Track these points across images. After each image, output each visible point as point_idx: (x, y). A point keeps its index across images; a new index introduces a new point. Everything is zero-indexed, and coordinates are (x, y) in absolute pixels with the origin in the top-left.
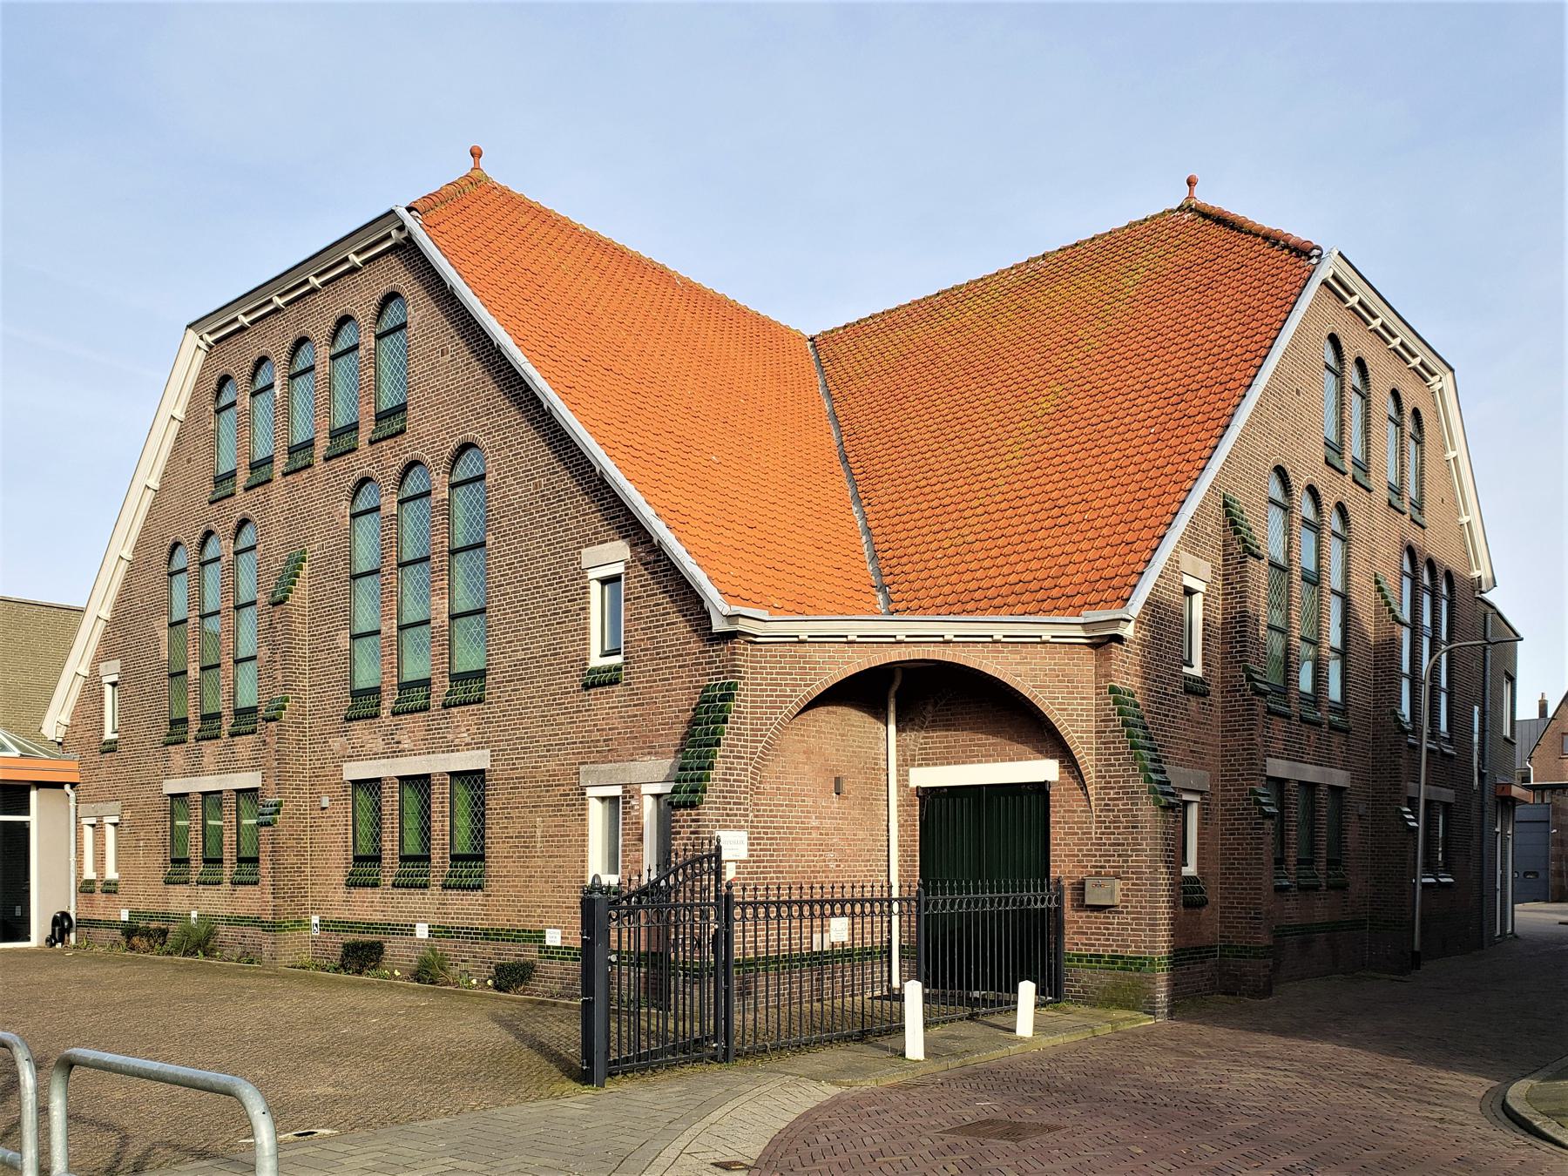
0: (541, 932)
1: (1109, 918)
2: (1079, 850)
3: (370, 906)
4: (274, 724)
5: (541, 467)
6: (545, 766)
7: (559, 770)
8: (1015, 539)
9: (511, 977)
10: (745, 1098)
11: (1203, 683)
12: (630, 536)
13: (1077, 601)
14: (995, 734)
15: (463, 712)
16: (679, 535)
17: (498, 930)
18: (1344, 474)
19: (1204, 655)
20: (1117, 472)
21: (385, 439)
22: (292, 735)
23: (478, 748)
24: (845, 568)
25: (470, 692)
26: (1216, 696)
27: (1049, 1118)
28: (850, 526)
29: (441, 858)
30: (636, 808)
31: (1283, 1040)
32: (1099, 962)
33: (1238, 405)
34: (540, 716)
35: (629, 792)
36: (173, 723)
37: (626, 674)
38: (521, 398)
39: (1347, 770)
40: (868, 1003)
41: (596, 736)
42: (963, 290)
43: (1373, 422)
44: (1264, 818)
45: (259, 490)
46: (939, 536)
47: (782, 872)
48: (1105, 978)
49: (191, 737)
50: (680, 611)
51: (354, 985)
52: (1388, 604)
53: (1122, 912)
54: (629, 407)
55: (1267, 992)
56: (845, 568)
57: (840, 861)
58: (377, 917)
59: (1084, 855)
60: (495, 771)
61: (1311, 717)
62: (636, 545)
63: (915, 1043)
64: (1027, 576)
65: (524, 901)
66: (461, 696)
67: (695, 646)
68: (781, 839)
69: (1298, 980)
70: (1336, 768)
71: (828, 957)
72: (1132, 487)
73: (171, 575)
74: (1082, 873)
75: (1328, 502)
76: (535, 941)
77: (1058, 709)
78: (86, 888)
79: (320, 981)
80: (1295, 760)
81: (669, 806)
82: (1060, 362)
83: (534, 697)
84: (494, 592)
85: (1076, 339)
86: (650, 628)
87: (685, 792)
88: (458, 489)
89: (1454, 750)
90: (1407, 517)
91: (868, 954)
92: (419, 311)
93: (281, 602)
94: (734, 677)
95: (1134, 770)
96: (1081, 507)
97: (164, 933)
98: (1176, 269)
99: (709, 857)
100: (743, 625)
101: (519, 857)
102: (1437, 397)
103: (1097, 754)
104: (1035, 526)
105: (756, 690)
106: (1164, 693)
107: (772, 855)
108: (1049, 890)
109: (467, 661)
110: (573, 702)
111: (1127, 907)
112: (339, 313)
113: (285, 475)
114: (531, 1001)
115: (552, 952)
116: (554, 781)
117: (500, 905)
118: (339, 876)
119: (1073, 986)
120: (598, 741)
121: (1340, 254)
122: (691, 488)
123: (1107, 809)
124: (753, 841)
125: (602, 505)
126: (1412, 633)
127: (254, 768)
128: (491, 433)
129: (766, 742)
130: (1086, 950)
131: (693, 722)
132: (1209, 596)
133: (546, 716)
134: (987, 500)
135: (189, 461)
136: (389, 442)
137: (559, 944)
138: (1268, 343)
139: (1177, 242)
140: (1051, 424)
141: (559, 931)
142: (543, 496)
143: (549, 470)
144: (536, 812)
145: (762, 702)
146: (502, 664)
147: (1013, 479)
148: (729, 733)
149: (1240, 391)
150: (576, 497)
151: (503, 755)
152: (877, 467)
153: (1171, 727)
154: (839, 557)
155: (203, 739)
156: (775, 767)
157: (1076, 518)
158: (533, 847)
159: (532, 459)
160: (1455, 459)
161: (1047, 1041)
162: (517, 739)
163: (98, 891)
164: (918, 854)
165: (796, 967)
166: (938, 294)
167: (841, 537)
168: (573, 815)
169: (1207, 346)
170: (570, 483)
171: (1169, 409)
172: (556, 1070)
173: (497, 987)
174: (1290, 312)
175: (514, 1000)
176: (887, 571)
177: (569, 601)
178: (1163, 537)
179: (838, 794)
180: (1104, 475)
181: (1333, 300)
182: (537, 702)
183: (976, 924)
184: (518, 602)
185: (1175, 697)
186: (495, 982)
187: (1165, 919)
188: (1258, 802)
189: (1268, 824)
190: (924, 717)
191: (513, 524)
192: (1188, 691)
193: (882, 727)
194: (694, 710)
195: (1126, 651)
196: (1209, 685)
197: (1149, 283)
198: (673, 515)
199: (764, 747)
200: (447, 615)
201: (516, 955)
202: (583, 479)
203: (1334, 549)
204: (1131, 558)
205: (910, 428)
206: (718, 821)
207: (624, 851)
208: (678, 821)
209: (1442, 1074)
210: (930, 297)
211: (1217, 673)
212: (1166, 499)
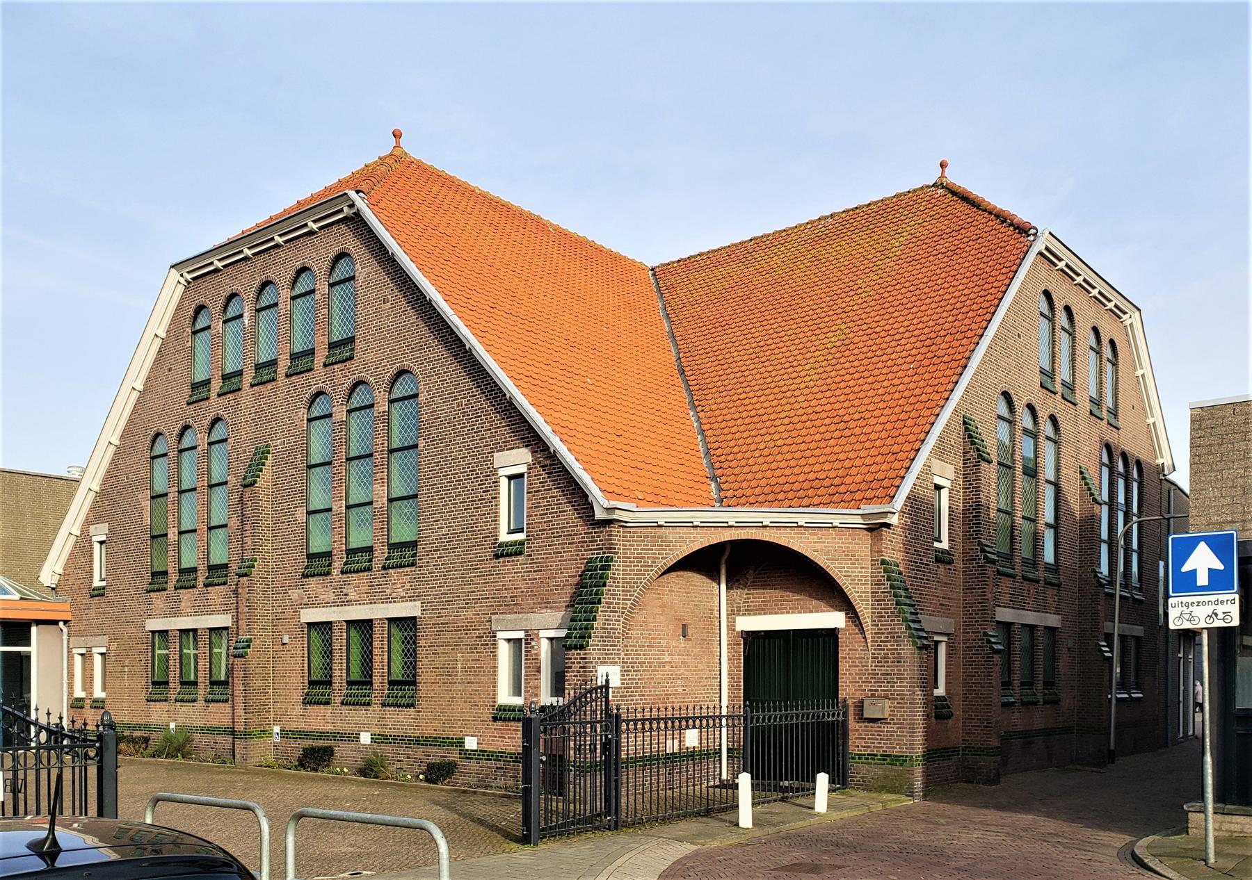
0: (461, 739)
1: (880, 727)
2: (859, 678)
3: (322, 719)
4: (245, 579)
5: (463, 391)
6: (464, 615)
7: (476, 618)
8: (813, 445)
9: (438, 773)
10: (635, 852)
11: (949, 554)
12: (531, 445)
13: (858, 496)
14: (799, 592)
15: (398, 573)
16: (570, 446)
17: (426, 737)
18: (1055, 393)
19: (950, 533)
20: (886, 397)
21: (336, 363)
22: (259, 587)
23: (411, 601)
24: (688, 464)
25: (404, 558)
26: (959, 563)
27: (838, 861)
28: (688, 428)
29: (381, 683)
30: (536, 647)
31: (1001, 813)
32: (873, 759)
33: (973, 350)
34: (461, 578)
35: (530, 635)
36: (154, 574)
37: (527, 548)
38: (447, 339)
39: (1058, 614)
40: (704, 791)
42: (770, 238)
43: (1077, 352)
44: (994, 653)
45: (231, 396)
46: (756, 439)
47: (644, 695)
48: (878, 771)
49: (171, 586)
50: (570, 502)
51: (313, 779)
52: (1089, 489)
53: (890, 723)
54: (527, 344)
55: (996, 781)
56: (688, 464)
57: (686, 686)
58: (329, 728)
59: (863, 682)
60: (425, 618)
61: (1030, 576)
62: (537, 452)
63: (746, 816)
64: (822, 475)
65: (448, 716)
66: (397, 561)
67: (581, 529)
69: (1022, 772)
70: (1050, 613)
71: (676, 757)
72: (897, 410)
73: (153, 458)
74: (861, 694)
75: (1043, 415)
76: (457, 746)
77: (845, 576)
78: (77, 704)
79: (286, 776)
80: (1018, 609)
81: (561, 647)
82: (844, 305)
83: (456, 563)
84: (424, 483)
85: (856, 287)
86: (546, 514)
87: (575, 637)
88: (396, 404)
89: (1143, 596)
90: (1105, 422)
91: (705, 754)
92: (365, 268)
93: (251, 485)
96: (860, 423)
97: (146, 740)
98: (931, 235)
99: (601, 687)
100: (618, 515)
101: (444, 683)
102: (1127, 330)
104: (827, 436)
106: (920, 563)
108: (838, 707)
109: (402, 533)
110: (486, 568)
111: (893, 719)
112: (298, 265)
113: (252, 386)
114: (456, 791)
115: (470, 754)
116: (471, 626)
117: (429, 719)
118: (297, 696)
119: (855, 777)
120: (506, 597)
121: (1050, 233)
122: (574, 407)
124: (624, 673)
125: (510, 421)
126: (1109, 509)
127: (225, 611)
128: (423, 363)
129: (634, 600)
130: (865, 751)
131: (580, 585)
132: (953, 490)
133: (465, 578)
134: (792, 413)
135: (169, 370)
136: (340, 365)
137: (475, 748)
138: (996, 302)
139: (932, 213)
140: (838, 355)
141: (476, 738)
142: (464, 412)
143: (469, 393)
144: (457, 649)
146: (429, 538)
147: (810, 397)
148: (607, 594)
149: (975, 340)
150: (490, 414)
151: (431, 606)
152: (708, 381)
153: (925, 587)
154: (683, 455)
155: (181, 588)
156: (640, 618)
157: (857, 431)
158: (455, 675)
159: (456, 385)
160: (1143, 375)
161: (837, 815)
162: (442, 594)
163: (87, 707)
164: (742, 680)
165: (654, 764)
166: (751, 240)
167: (683, 438)
168: (486, 652)
169: (952, 301)
170: (486, 405)
171: (924, 350)
172: (499, 836)
173: (428, 780)
174: (1013, 278)
175: (443, 790)
176: (717, 465)
177: (483, 492)
178: (919, 450)
179: (684, 637)
180: (877, 399)
181: (1046, 264)
182: (458, 567)
183: (786, 732)
184: (443, 491)
185: (928, 565)
186: (426, 777)
187: (921, 728)
188: (989, 642)
189: (997, 658)
190: (747, 579)
191: (440, 432)
192: (938, 560)
193: (716, 586)
194: (580, 576)
195: (893, 533)
196: (953, 555)
197: (911, 245)
198: (564, 431)
199: (632, 604)
200: (386, 499)
201: (442, 756)
202: (495, 401)
203: (1048, 450)
204: (896, 465)
205: (732, 350)
206: (599, 659)
207: (526, 679)
208: (570, 659)
209: (1101, 833)
210: (745, 242)
211: (960, 546)
212: (921, 421)
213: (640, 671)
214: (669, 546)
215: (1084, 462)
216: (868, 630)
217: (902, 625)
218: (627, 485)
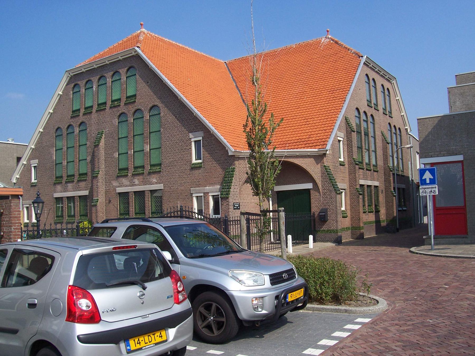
11: (344, 162)
26: (347, 166)
41: (195, 180)
43: (378, 93)
68: (246, 205)
75: (369, 115)
87: (225, 194)
90: (388, 115)
94: (235, 166)
103: (322, 182)
123: (324, 194)
127: (86, 190)
145: (241, 172)
189: (361, 196)
192: (341, 165)
211: (347, 160)
218: (237, 143)
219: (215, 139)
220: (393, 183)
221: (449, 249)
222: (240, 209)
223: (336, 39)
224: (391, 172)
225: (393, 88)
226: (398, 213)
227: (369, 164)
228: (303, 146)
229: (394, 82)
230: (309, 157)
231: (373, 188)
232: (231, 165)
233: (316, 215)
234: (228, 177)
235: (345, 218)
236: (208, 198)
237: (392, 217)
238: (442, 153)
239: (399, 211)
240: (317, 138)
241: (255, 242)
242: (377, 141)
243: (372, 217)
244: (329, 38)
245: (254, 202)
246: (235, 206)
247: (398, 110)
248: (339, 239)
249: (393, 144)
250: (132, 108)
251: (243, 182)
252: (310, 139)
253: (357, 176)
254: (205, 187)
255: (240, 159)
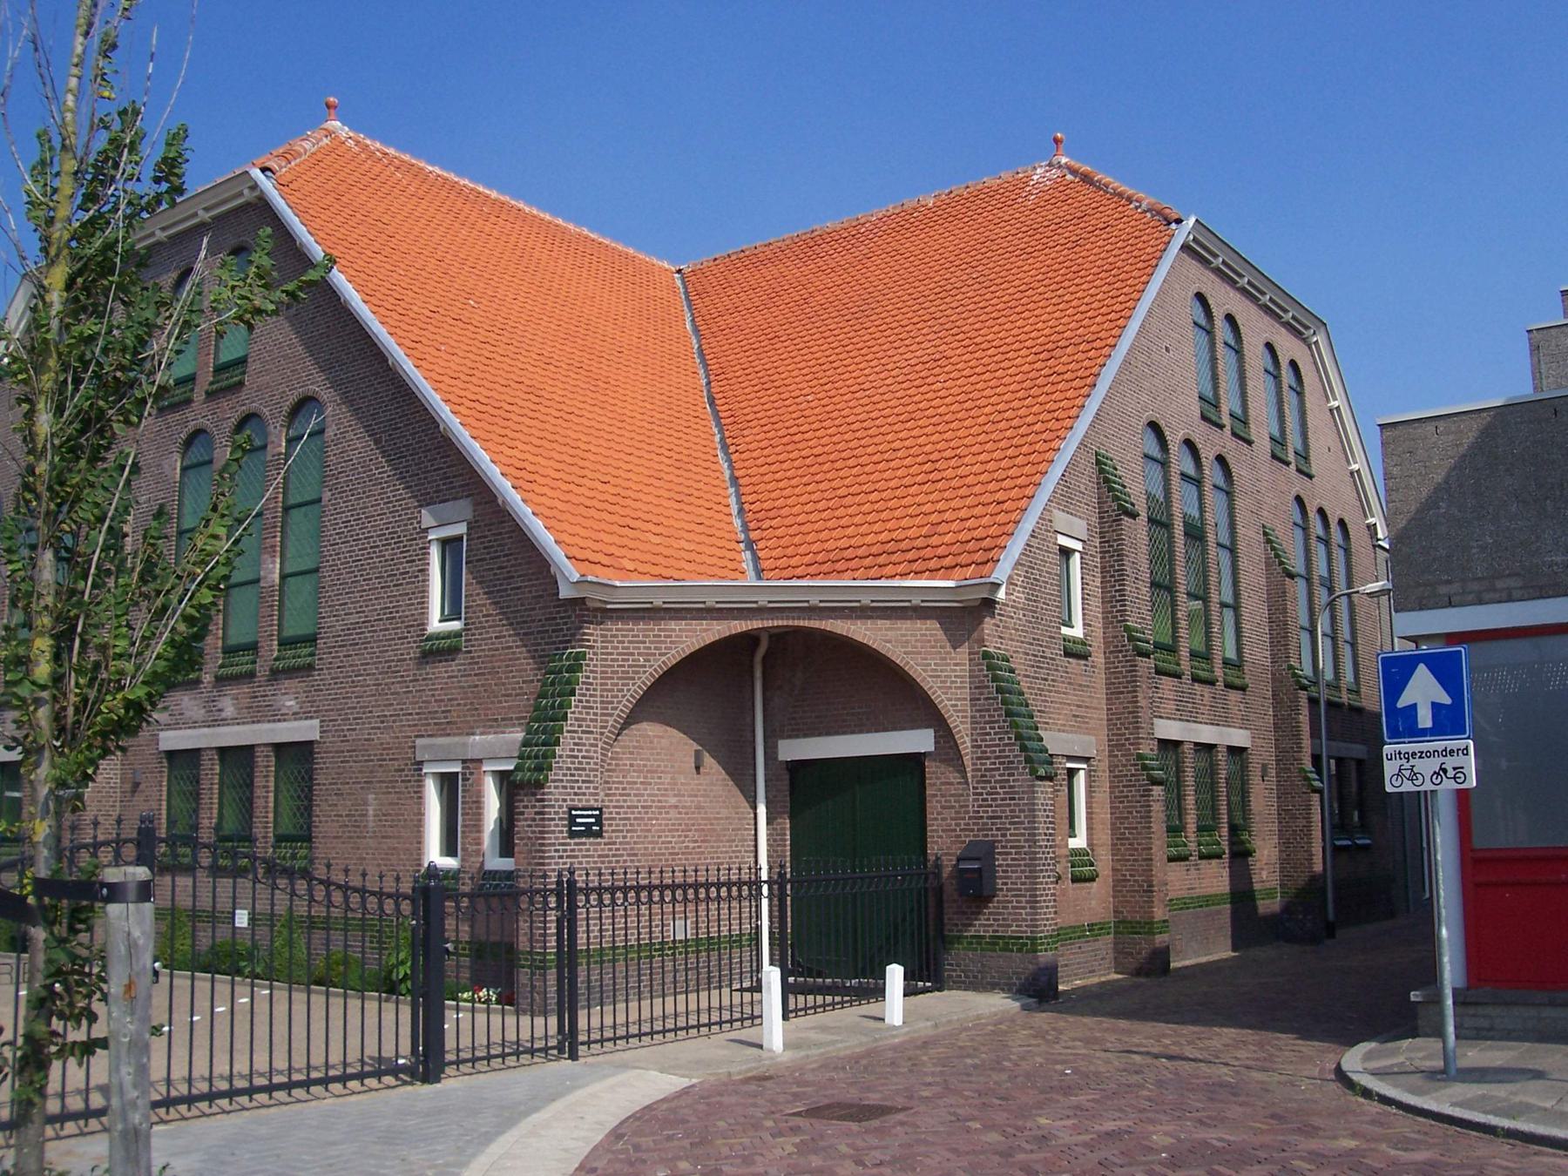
19: (1084, 614)
26: (1098, 658)
41: (434, 707)
43: (1248, 375)
44: (1154, 783)
47: (636, 855)
62: (480, 504)
75: (1207, 455)
77: (931, 676)
87: (529, 770)
90: (1293, 466)
95: (1010, 739)
103: (972, 723)
105: (606, 660)
107: (624, 837)
123: (983, 780)
153: (1050, 691)
158: (365, 826)
189: (1157, 790)
192: (1068, 654)
198: (519, 474)
207: (463, 832)
211: (1099, 633)
213: (629, 819)
214: (670, 636)
215: (1267, 517)
216: (967, 754)
217: (1013, 744)
219: (513, 531)
220: (1312, 736)
221: (1538, 1075)
222: (601, 837)
223: (1085, 168)
224: (1303, 694)
225: (1315, 363)
226: (1334, 857)
227: (1202, 656)
228: (900, 569)
229: (1320, 338)
230: (920, 613)
231: (1222, 756)
232: (569, 641)
233: (946, 871)
234: (553, 696)
235: (1088, 884)
236: (479, 783)
237: (1302, 880)
238: (1499, 584)
239: (1337, 850)
240: (963, 536)
241: (675, 982)
242: (1243, 563)
243: (1215, 878)
244: (1060, 167)
245: (676, 807)
246: (578, 820)
247: (1336, 446)
248: (1044, 979)
249: (1316, 580)
250: (231, 410)
251: (619, 716)
252: (934, 541)
253: (1143, 703)
254: (468, 734)
255: (611, 618)
